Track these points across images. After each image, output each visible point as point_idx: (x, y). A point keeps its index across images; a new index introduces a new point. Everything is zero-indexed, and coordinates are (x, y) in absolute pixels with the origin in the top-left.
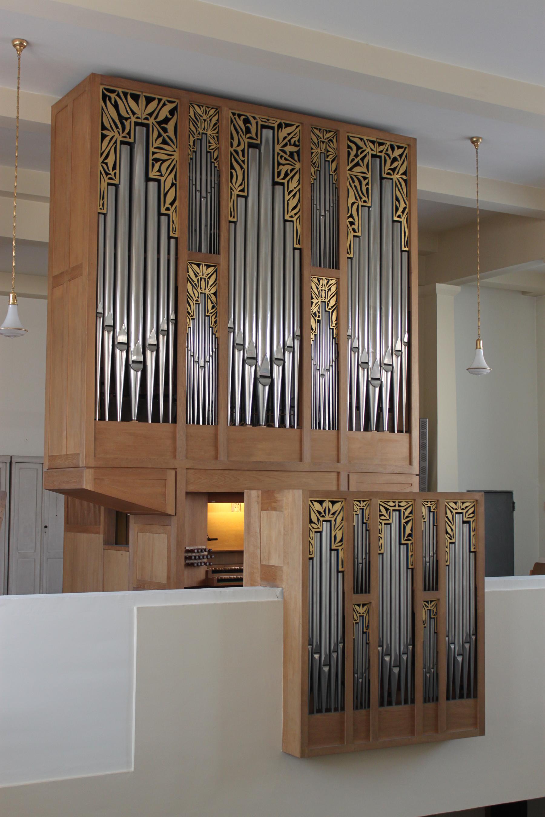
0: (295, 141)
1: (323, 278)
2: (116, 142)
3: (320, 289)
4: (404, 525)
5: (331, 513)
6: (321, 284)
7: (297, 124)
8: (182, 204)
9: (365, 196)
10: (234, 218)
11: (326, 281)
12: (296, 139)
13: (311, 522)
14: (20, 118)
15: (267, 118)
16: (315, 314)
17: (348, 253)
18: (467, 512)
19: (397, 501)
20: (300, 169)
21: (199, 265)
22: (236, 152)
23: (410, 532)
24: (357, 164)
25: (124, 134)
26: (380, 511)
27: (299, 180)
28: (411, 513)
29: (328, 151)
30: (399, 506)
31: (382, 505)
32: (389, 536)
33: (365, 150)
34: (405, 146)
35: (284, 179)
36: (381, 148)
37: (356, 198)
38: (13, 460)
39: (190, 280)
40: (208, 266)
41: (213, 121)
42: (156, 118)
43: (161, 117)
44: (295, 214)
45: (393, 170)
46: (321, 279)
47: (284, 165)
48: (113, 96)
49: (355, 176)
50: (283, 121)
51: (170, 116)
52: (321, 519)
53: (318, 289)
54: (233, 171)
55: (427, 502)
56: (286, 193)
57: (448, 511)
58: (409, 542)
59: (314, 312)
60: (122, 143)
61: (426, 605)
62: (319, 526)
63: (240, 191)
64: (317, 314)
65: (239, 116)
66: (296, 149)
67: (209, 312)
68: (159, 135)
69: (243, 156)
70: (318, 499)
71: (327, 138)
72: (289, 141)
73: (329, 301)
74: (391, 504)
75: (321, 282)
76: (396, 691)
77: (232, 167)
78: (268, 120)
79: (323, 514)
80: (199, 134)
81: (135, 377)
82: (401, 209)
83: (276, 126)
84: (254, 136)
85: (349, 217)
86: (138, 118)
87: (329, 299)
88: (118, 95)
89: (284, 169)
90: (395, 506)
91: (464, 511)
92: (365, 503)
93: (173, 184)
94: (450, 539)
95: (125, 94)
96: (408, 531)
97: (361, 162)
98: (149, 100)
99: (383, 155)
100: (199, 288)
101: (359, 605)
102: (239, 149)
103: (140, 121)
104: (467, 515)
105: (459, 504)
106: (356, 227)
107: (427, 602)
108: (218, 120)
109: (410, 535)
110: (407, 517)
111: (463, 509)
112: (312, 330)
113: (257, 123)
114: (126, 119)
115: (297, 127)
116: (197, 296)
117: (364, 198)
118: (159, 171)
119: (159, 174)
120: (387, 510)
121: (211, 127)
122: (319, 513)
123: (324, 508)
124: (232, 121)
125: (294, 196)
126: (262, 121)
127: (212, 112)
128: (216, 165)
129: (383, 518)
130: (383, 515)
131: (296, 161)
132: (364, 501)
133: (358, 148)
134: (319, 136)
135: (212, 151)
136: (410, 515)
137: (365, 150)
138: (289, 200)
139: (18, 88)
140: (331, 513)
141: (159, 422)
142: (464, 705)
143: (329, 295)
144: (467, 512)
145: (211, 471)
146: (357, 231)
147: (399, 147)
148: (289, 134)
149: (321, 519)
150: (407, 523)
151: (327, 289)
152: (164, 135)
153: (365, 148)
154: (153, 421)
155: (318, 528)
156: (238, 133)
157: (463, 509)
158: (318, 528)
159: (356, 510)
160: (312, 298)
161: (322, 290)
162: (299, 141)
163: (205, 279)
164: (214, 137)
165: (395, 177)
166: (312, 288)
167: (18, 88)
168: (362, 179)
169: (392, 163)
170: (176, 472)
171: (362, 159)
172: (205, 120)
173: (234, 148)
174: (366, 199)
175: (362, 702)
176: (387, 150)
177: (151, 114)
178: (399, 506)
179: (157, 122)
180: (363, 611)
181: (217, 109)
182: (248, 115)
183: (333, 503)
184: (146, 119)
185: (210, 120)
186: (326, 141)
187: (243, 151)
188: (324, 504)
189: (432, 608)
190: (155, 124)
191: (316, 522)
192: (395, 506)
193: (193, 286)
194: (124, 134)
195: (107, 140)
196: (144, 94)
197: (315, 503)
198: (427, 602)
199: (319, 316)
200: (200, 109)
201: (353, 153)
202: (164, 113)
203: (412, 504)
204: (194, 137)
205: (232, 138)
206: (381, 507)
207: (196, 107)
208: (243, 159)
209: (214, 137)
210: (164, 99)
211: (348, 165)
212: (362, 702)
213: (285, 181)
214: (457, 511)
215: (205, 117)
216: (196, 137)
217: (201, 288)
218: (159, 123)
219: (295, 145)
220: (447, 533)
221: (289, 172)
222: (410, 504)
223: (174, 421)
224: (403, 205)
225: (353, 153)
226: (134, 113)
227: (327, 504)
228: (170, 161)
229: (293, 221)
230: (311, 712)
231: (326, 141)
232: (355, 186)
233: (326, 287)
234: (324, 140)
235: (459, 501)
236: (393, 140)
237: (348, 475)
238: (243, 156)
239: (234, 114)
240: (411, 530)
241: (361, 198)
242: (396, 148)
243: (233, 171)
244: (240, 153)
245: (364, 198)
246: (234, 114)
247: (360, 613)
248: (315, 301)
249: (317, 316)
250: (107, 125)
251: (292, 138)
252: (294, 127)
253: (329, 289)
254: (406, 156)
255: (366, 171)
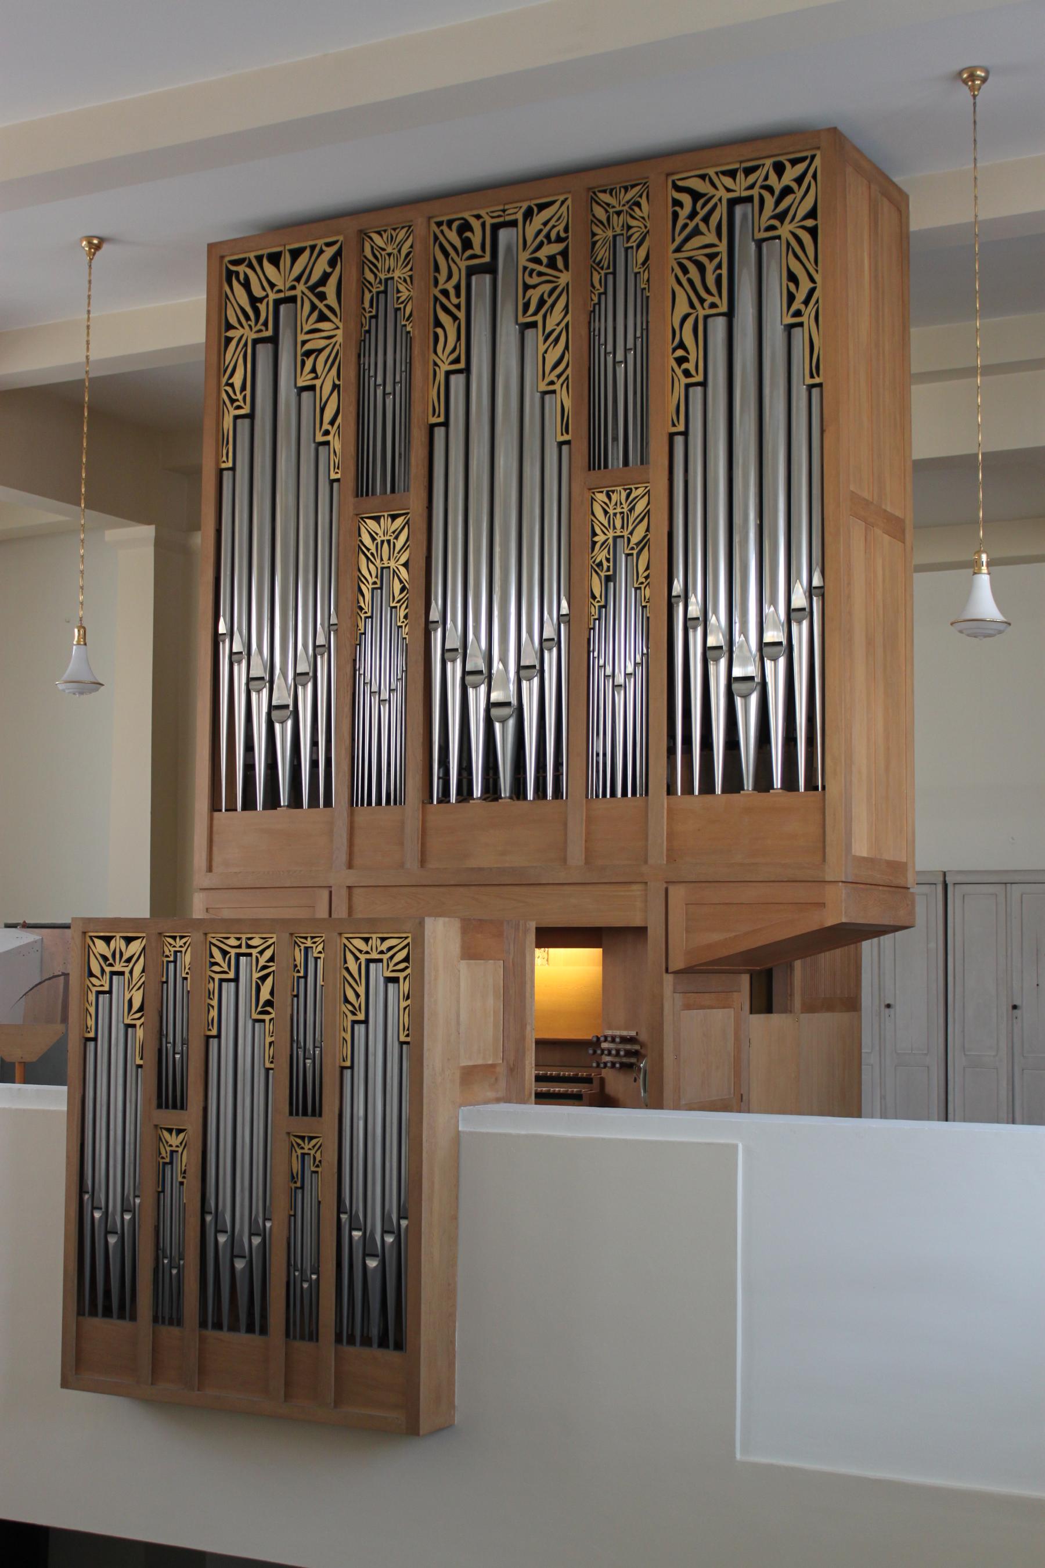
0: (558, 232)
1: (619, 488)
2: (246, 345)
3: (611, 512)
4: (257, 983)
5: (125, 958)
6: (613, 502)
7: (562, 198)
8: (347, 421)
9: (712, 294)
10: (439, 416)
11: (624, 494)
12: (561, 227)
13: (91, 974)
14: (91, 358)
15: (501, 208)
16: (600, 564)
17: (674, 425)
18: (392, 957)
19: (244, 937)
20: (568, 284)
21: (377, 519)
22: (445, 293)
23: (269, 997)
24: (697, 232)
25: (259, 327)
26: (212, 956)
27: (567, 306)
28: (272, 959)
29: (629, 228)
30: (249, 946)
31: (215, 945)
32: (234, 1007)
33: (713, 196)
34: (809, 154)
35: (535, 313)
36: (752, 179)
37: (692, 306)
38: (947, 879)
39: (361, 548)
40: (394, 517)
41: (405, 251)
42: (306, 283)
43: (315, 277)
44: (559, 376)
45: (781, 217)
46: (613, 492)
47: (534, 287)
48: (241, 269)
49: (690, 259)
50: (533, 203)
51: (329, 270)
52: (108, 969)
53: (606, 512)
54: (439, 331)
55: (306, 938)
56: (541, 339)
57: (350, 958)
58: (267, 1017)
59: (598, 561)
60: (256, 342)
61: (299, 1145)
62: (103, 983)
63: (452, 363)
64: (605, 564)
65: (450, 223)
66: (560, 247)
67: (396, 600)
68: (314, 307)
69: (458, 296)
70: (102, 934)
71: (628, 202)
72: (548, 236)
73: (631, 533)
74: (233, 942)
75: (614, 497)
76: (234, 1303)
77: (438, 324)
78: (504, 211)
79: (111, 961)
80: (380, 282)
81: (283, 733)
82: (801, 296)
83: (520, 217)
84: (477, 250)
85: (674, 350)
86: (280, 291)
87: (630, 528)
88: (250, 266)
89: (534, 295)
90: (240, 946)
91: (385, 957)
92: (184, 940)
93: (335, 386)
94: (354, 1014)
95: (259, 259)
96: (265, 995)
97: (703, 227)
98: (296, 254)
99: (755, 192)
100: (378, 561)
101: (170, 1131)
102: (450, 287)
103: (282, 295)
104: (391, 965)
105: (374, 942)
106: (690, 366)
107: (303, 1138)
108: (411, 247)
109: (269, 1003)
110: (264, 967)
111: (382, 952)
112: (594, 597)
113: (483, 225)
114: (261, 300)
115: (563, 203)
116: (374, 575)
117: (710, 299)
118: (314, 370)
119: (313, 375)
120: (225, 953)
121: (400, 264)
122: (105, 958)
123: (112, 949)
124: (436, 238)
125: (557, 340)
126: (492, 217)
127: (402, 234)
128: (409, 329)
129: (216, 968)
130: (217, 964)
131: (561, 271)
132: (182, 937)
133: (696, 196)
134: (608, 205)
135: (402, 306)
136: (271, 964)
137: (713, 196)
138: (546, 352)
139: (89, 312)
140: (125, 958)
141: (301, 807)
142: (372, 1362)
143: (631, 521)
144: (392, 957)
145: (395, 889)
146: (693, 372)
147: (794, 162)
148: (545, 224)
149: (108, 969)
150: (263, 979)
151: (625, 510)
152: (321, 306)
153: (711, 191)
154: (310, 806)
155: (102, 986)
156: (446, 254)
157: (382, 952)
158: (102, 986)
159: (167, 953)
160: (594, 534)
161: (615, 514)
162: (566, 230)
163: (389, 541)
164: (405, 281)
165: (785, 230)
166: (593, 514)
167: (89, 312)
168: (705, 260)
169: (777, 203)
170: (331, 892)
171: (706, 220)
172: (389, 255)
173: (440, 287)
174: (716, 300)
175: (302, 1326)
176: (766, 178)
177: (298, 279)
178: (249, 946)
179: (308, 288)
180: (178, 1143)
181: (410, 227)
182: (466, 215)
183: (129, 940)
184: (293, 288)
185: (399, 251)
186: (626, 208)
187: (457, 288)
188: (113, 942)
189: (312, 1152)
190: (306, 291)
191: (99, 975)
192: (240, 946)
193: (368, 558)
194: (259, 327)
195: (234, 343)
196: (288, 247)
197: (98, 942)
198: (303, 1138)
199: (609, 567)
200: (381, 236)
201: (684, 213)
202: (322, 266)
203: (408, 944)
204: (370, 291)
205: (437, 269)
206: (213, 948)
207: (375, 236)
208: (455, 301)
209: (405, 281)
210: (320, 243)
211: (673, 240)
212: (302, 1326)
213: (539, 318)
214: (368, 956)
215: (389, 250)
216: (374, 291)
217: (382, 560)
218: (312, 289)
219: (559, 239)
220: (346, 1001)
221: (546, 297)
222: (271, 941)
223: (328, 803)
224: (805, 285)
225: (684, 213)
226: (272, 285)
227: (118, 943)
228: (330, 347)
229: (554, 392)
230: (80, 1312)
231: (626, 208)
232: (691, 282)
233: (625, 506)
234: (621, 208)
235: (374, 936)
236: (791, 149)
237: (667, 890)
238: (458, 296)
239: (439, 224)
240: (272, 993)
241: (702, 301)
242: (788, 165)
243: (439, 331)
244: (452, 292)
245: (710, 299)
246: (439, 224)
247: (171, 1146)
248: (600, 538)
249: (605, 568)
250: (233, 321)
251: (554, 226)
252: (558, 204)
253: (632, 510)
254: (814, 176)
255: (716, 241)
